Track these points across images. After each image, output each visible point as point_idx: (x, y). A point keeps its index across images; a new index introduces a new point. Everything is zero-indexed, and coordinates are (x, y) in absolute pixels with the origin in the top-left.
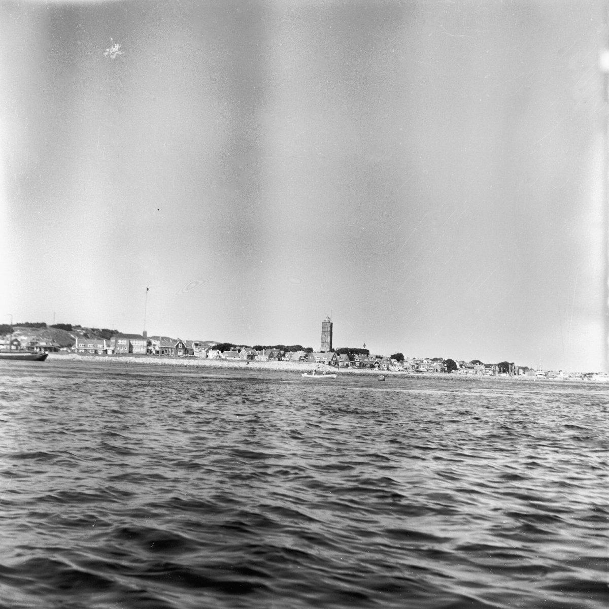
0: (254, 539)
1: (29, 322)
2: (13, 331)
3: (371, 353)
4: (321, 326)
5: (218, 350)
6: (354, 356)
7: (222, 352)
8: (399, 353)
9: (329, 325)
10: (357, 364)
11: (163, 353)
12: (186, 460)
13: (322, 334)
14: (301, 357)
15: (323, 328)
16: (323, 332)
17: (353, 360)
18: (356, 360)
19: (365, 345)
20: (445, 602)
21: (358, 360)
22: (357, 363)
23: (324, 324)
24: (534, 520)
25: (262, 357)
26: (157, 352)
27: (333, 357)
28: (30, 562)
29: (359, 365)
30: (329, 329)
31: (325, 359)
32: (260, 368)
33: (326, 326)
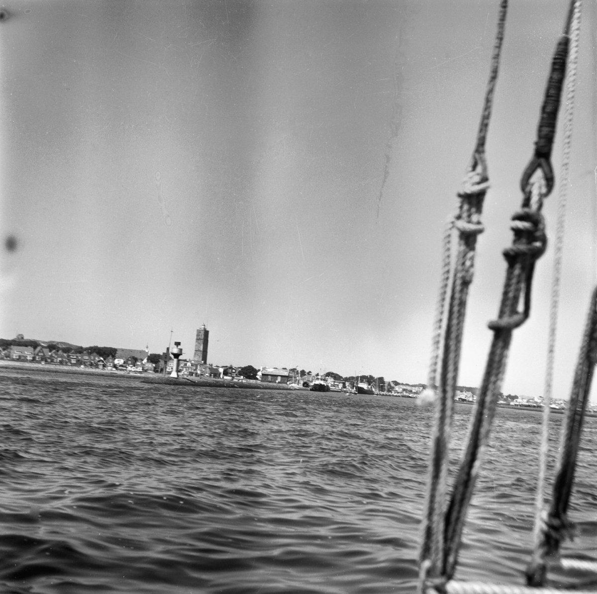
4: (195, 333)
9: (203, 333)
10: (73, 361)
13: (196, 342)
15: (197, 335)
16: (197, 339)
21: (75, 357)
22: (72, 360)
23: (199, 332)
29: (75, 362)
30: (203, 337)
33: (200, 334)
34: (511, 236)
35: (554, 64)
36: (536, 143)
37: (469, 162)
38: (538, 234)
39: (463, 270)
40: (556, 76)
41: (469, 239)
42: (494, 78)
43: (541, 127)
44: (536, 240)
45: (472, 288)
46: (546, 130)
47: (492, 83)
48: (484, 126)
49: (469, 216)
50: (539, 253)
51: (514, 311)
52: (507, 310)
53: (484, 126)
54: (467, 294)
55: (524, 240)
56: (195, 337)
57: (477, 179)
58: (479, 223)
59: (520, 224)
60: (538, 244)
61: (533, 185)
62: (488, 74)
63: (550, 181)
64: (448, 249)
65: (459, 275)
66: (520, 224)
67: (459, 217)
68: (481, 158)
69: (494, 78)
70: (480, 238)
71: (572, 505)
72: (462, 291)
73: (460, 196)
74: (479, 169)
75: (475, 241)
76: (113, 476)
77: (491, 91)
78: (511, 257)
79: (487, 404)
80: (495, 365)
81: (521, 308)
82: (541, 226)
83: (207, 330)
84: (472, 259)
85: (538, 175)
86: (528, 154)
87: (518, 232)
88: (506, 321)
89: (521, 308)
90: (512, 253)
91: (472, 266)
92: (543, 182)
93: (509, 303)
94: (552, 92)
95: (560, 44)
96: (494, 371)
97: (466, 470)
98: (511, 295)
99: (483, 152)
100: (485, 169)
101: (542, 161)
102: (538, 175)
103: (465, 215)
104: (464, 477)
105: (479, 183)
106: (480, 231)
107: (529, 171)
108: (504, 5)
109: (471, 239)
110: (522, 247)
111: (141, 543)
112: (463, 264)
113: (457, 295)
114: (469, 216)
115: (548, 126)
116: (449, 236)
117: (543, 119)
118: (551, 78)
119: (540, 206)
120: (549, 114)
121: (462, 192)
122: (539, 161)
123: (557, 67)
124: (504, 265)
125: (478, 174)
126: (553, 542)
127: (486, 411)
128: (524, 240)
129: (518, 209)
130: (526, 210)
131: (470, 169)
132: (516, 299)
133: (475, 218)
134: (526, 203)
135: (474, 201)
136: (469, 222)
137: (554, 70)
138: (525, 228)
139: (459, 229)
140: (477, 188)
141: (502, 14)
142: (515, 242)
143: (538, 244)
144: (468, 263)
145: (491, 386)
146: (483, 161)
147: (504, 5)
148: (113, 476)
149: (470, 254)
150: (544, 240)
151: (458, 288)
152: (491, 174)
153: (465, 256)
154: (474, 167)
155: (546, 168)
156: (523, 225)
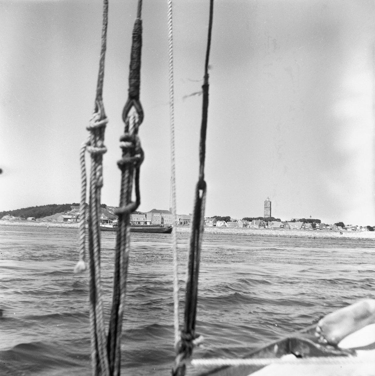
0: (5, 332)
1: (76, 203)
2: (71, 209)
3: (322, 222)
5: (224, 221)
6: (315, 225)
7: (226, 222)
8: (341, 222)
9: (269, 203)
11: (185, 224)
12: (320, 290)
13: (265, 209)
14: (281, 225)
15: (265, 205)
16: (265, 207)
17: (315, 228)
18: (317, 227)
19: (311, 217)
20: (47, 357)
21: (319, 227)
23: (266, 203)
24: (276, 305)
25: (254, 225)
26: (181, 223)
27: (302, 225)
28: (236, 349)
30: (269, 205)
31: (297, 227)
32: (359, 238)
34: (120, 152)
35: (134, 37)
36: (129, 90)
37: (93, 107)
38: (137, 149)
39: (95, 179)
40: (136, 45)
41: (97, 157)
42: (104, 50)
43: (130, 79)
44: (137, 153)
45: (103, 190)
46: (133, 81)
47: (103, 54)
48: (100, 83)
49: (95, 142)
50: (140, 161)
51: (129, 201)
52: (124, 200)
53: (100, 83)
54: (100, 194)
55: (128, 154)
56: (264, 206)
57: (98, 117)
58: (102, 146)
59: (124, 144)
60: (138, 156)
61: (129, 117)
62: (100, 48)
63: (141, 113)
64: (84, 165)
65: (93, 182)
66: (124, 144)
67: (89, 144)
68: (100, 104)
69: (104, 50)
70: (105, 156)
71: (367, 292)
72: (96, 192)
73: (89, 129)
74: (99, 111)
75: (101, 159)
76: (275, 289)
77: (103, 59)
78: (122, 166)
79: (121, 266)
80: (122, 239)
81: (134, 198)
82: (137, 144)
83: (271, 201)
84: (101, 170)
85: (133, 110)
86: (124, 98)
87: (125, 149)
88: (124, 208)
89: (134, 198)
90: (121, 163)
91: (101, 175)
92: (137, 115)
93: (125, 196)
94: (135, 56)
95: (135, 24)
96: (122, 243)
97: (115, 311)
98: (125, 191)
99: (102, 99)
100: (103, 110)
101: (134, 101)
102: (133, 110)
103: (93, 142)
104: (114, 317)
105: (99, 120)
106: (105, 152)
107: (127, 109)
108: (106, 3)
109: (98, 158)
110: (128, 159)
111: (262, 331)
112: (95, 174)
113: (93, 196)
114: (95, 142)
115: (134, 78)
116: (83, 156)
117: (131, 74)
118: (133, 47)
119: (136, 131)
120: (134, 70)
121: (88, 127)
122: (131, 102)
123: (135, 39)
124: (119, 172)
125: (99, 114)
126: (187, 349)
127: (121, 270)
128: (128, 154)
129: (122, 133)
130: (127, 134)
131: (94, 111)
132: (129, 194)
133: (99, 143)
134: (127, 130)
135: (98, 132)
136: (96, 146)
137: (134, 41)
138: (127, 146)
139: (89, 152)
140: (98, 123)
141: (105, 8)
142: (123, 155)
143: (138, 156)
144: (98, 174)
145: (122, 253)
146: (102, 106)
147: (106, 3)
148: (275, 289)
149: (99, 167)
150: (141, 152)
151: (94, 191)
152: (107, 113)
153: (95, 169)
154: (97, 110)
155: (137, 106)
156: (126, 145)
